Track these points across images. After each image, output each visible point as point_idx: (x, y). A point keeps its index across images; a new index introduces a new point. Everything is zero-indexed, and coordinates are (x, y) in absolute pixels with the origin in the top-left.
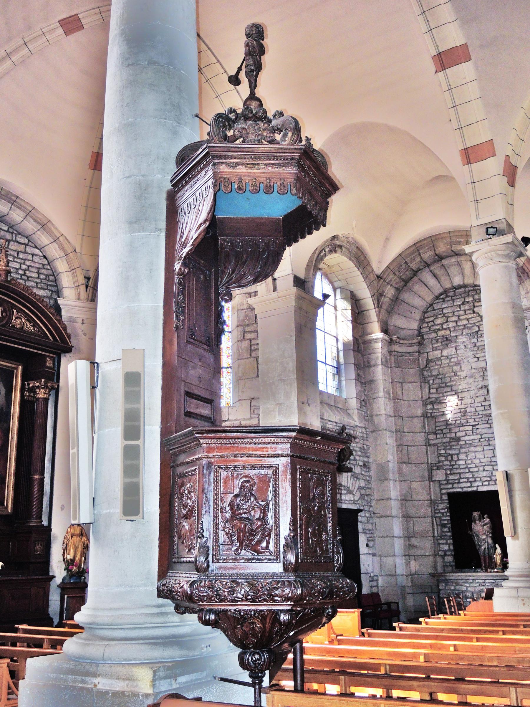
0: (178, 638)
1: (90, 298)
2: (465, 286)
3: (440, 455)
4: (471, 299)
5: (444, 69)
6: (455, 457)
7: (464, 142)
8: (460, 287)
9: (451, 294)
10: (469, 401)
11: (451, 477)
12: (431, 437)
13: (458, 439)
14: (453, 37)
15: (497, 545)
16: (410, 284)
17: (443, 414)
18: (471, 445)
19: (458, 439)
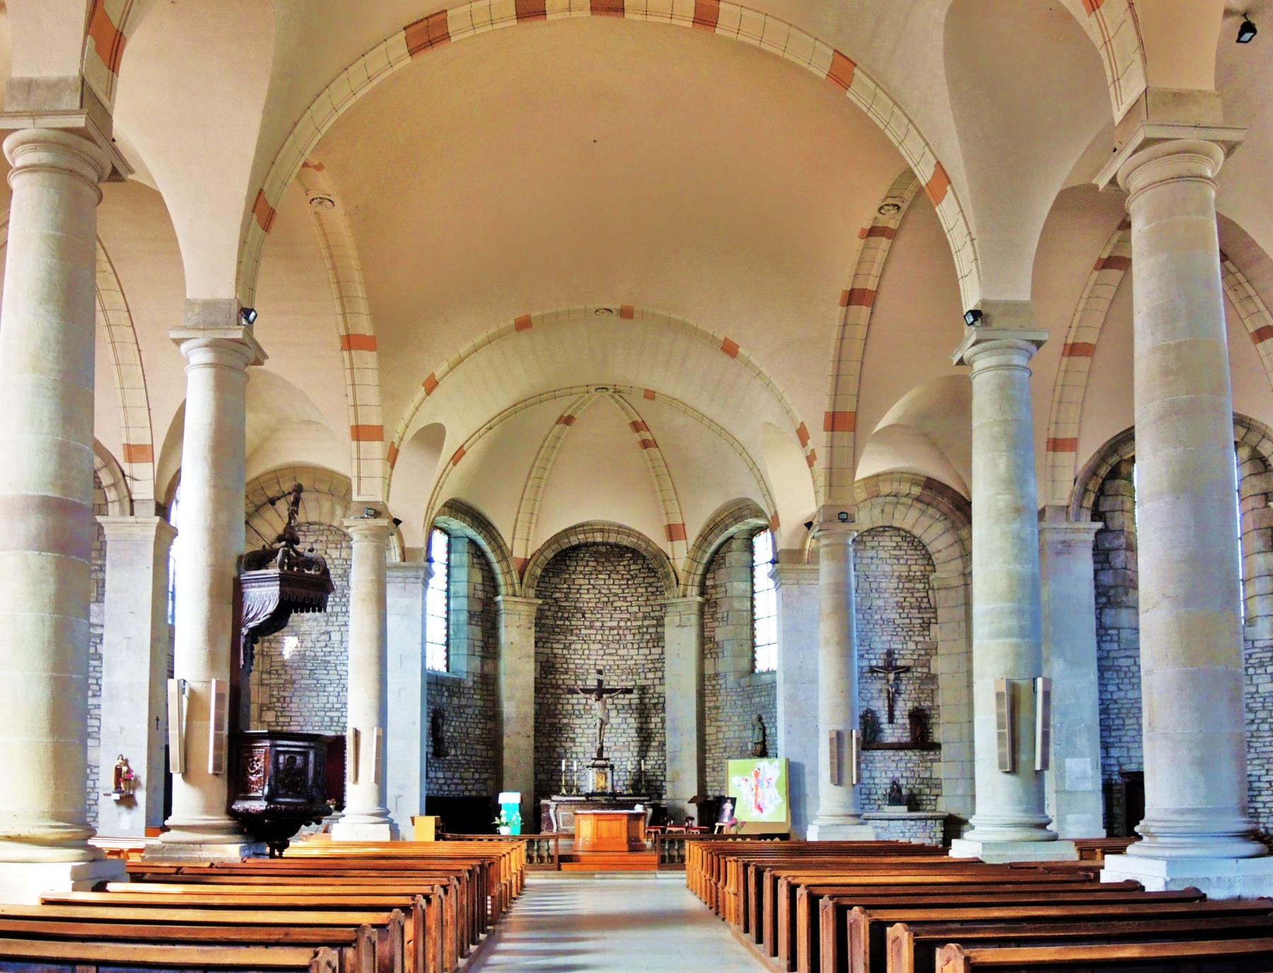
0: (708, 607)
1: (728, 806)
2: (320, 524)
3: (272, 696)
4: (324, 539)
5: (350, 349)
6: (288, 700)
7: (356, 419)
8: (315, 523)
9: (304, 528)
10: (310, 644)
11: (281, 719)
12: (265, 676)
13: (293, 682)
14: (364, 327)
15: (1118, 116)
16: (262, 510)
17: (281, 654)
18: (306, 689)
19: (293, 682)
